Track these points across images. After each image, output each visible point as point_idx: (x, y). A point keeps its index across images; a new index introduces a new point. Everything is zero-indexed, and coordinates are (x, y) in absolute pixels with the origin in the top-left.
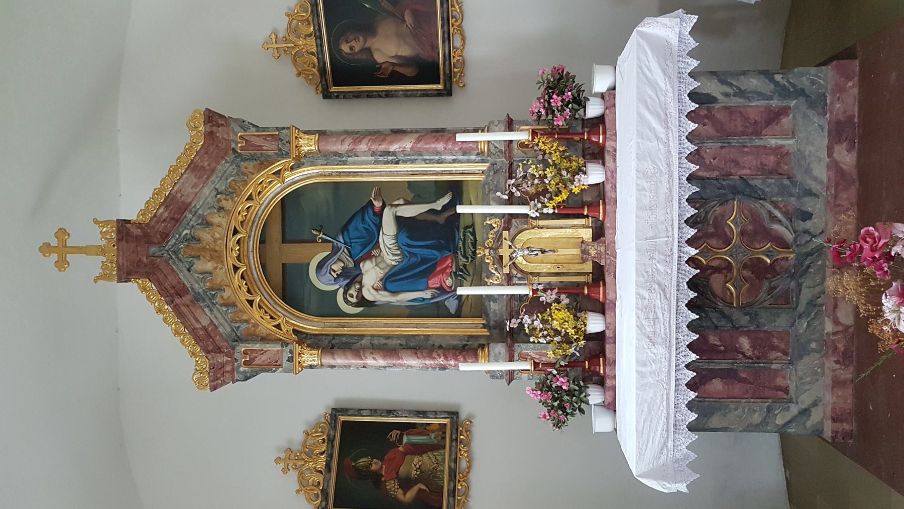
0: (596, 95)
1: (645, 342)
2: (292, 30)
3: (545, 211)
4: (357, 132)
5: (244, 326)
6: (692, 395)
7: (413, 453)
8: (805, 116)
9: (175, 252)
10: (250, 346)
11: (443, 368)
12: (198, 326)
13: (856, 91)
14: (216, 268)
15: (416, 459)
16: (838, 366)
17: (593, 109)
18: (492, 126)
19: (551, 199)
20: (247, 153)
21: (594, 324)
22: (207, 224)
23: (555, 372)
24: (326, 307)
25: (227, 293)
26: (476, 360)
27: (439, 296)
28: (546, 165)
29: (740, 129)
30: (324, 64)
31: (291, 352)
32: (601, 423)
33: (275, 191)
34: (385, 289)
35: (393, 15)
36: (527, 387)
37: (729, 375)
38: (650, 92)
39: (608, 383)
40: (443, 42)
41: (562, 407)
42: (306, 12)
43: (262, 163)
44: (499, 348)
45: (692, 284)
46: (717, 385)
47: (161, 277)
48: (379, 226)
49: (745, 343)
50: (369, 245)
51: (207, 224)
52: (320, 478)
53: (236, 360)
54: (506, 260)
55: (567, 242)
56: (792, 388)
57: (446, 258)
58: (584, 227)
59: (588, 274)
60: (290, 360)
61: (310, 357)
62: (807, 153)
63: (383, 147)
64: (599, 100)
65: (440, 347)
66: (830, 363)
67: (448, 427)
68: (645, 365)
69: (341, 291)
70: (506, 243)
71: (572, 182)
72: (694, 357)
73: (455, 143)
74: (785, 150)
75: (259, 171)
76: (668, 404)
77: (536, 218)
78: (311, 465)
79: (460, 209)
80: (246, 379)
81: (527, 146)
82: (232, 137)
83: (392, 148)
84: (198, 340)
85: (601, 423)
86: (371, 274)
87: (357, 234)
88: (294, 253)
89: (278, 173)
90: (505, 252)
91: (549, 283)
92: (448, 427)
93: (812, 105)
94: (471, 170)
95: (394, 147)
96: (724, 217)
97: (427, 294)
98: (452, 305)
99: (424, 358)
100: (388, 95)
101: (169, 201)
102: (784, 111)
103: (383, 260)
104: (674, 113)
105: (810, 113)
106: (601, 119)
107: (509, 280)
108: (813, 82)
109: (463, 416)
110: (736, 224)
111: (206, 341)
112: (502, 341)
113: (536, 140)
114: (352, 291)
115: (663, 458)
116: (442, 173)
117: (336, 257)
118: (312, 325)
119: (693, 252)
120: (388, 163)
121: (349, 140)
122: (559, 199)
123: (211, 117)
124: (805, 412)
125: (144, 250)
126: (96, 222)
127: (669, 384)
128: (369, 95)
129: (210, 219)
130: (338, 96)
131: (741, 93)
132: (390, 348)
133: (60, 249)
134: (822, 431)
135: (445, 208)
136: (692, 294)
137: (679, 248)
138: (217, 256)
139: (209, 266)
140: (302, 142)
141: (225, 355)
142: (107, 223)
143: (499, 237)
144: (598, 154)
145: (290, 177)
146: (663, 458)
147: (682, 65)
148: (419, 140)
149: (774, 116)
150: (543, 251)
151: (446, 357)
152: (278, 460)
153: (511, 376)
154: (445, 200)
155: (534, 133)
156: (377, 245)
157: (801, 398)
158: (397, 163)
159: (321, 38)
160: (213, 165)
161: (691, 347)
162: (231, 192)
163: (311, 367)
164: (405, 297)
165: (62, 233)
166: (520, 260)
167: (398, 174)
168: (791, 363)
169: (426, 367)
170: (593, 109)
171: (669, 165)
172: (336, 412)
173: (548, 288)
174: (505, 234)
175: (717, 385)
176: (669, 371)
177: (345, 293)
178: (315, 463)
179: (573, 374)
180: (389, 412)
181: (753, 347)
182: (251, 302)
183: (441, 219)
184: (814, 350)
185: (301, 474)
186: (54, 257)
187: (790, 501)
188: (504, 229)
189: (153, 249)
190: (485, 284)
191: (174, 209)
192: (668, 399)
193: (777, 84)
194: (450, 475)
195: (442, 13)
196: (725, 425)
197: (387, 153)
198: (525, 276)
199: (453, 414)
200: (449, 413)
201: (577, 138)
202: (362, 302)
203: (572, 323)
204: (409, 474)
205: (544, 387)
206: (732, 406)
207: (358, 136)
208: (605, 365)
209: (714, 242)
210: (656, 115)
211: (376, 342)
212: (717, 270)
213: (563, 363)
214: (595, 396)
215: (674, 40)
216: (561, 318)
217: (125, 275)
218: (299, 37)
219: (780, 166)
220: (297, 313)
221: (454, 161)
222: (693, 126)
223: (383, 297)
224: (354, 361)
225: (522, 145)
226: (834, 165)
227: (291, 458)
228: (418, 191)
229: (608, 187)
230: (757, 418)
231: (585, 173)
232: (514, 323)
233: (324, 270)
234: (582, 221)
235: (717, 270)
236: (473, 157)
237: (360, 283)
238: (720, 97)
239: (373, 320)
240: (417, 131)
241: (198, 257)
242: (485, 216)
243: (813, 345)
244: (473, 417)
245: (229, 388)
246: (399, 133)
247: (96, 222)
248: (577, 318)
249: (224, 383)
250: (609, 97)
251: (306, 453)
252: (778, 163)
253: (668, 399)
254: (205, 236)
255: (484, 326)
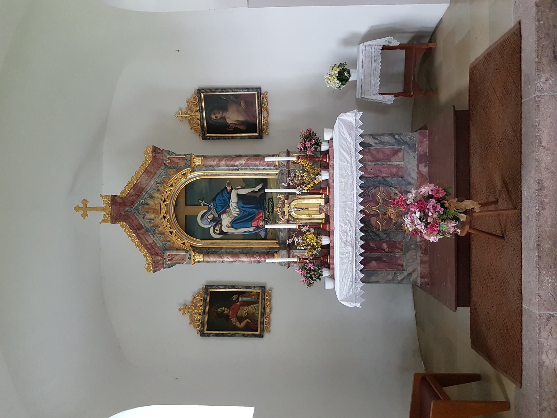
0: (326, 141)
1: (343, 245)
2: (189, 108)
3: (303, 191)
4: (220, 156)
5: (169, 243)
6: (362, 267)
7: (245, 306)
8: (408, 152)
9: (137, 210)
10: (171, 252)
11: (259, 262)
12: (147, 243)
13: (427, 142)
14: (156, 217)
15: (245, 308)
16: (422, 255)
17: (324, 147)
18: (281, 154)
19: (306, 186)
20: (171, 165)
21: (325, 241)
22: (152, 197)
23: (308, 262)
24: (205, 235)
25: (161, 229)
26: (274, 258)
27: (257, 230)
28: (304, 171)
29: (382, 157)
30: (204, 124)
31: (190, 255)
32: (328, 285)
33: (182, 182)
34: (232, 227)
35: (235, 102)
36: (296, 270)
37: (379, 259)
38: (344, 143)
39: (331, 266)
40: (259, 115)
41: (311, 277)
42: (196, 100)
43: (177, 170)
44: (284, 252)
45: (362, 221)
46: (374, 263)
47: (131, 221)
48: (230, 198)
49: (385, 246)
50: (225, 207)
51: (152, 197)
52: (200, 317)
53: (165, 259)
54: (286, 213)
55: (314, 205)
56: (404, 264)
57: (260, 213)
58: (321, 198)
59: (322, 219)
60: (190, 258)
61: (199, 258)
62: (409, 167)
63: (232, 163)
64: (327, 143)
65: (257, 253)
66: (419, 254)
67: (261, 293)
68: (343, 254)
69: (212, 228)
70: (286, 206)
71: (315, 179)
72: (363, 251)
73: (264, 161)
74: (400, 166)
75: (176, 174)
76: (352, 271)
77: (299, 195)
78: (196, 311)
79: (266, 191)
80: (170, 267)
81: (296, 163)
82: (164, 158)
83: (236, 163)
84: (148, 249)
85: (328, 285)
86: (226, 220)
87: (219, 202)
88: (190, 211)
89: (184, 174)
90: (286, 209)
91: (306, 223)
92: (261, 293)
93: (410, 148)
94: (271, 174)
95: (237, 163)
96: (376, 194)
97: (251, 229)
98: (263, 234)
99: (250, 257)
100: (233, 138)
101: (135, 187)
102: (400, 150)
103: (231, 214)
104: (354, 151)
105: (409, 151)
106: (327, 152)
107: (288, 222)
108: (411, 139)
109: (268, 288)
110: (380, 197)
111: (151, 250)
112: (285, 249)
113: (299, 161)
114: (217, 228)
115: (351, 293)
116: (258, 175)
117: (210, 212)
118: (199, 244)
119: (362, 207)
120: (234, 170)
121: (217, 160)
122: (309, 186)
123: (155, 150)
124: (410, 274)
125: (124, 209)
126: (101, 196)
127: (353, 262)
128: (224, 138)
129: (153, 195)
130: (209, 138)
131: (381, 143)
132: (234, 253)
133: (84, 209)
134: (417, 283)
135: (259, 190)
136: (362, 225)
137: (357, 206)
138: (156, 212)
139: (153, 216)
140: (196, 161)
141: (160, 256)
142: (106, 196)
143: (284, 203)
144: (326, 167)
145: (190, 176)
146: (351, 293)
147: (356, 132)
148: (248, 160)
149: (395, 152)
150: (302, 209)
151: (260, 257)
152: (180, 309)
153: (289, 264)
154: (260, 187)
155: (299, 157)
156: (229, 207)
157: (408, 269)
158: (238, 170)
159: (202, 112)
160: (155, 171)
161: (362, 247)
162: (163, 183)
163: (198, 262)
164: (242, 230)
165: (85, 201)
166: (293, 213)
167: (238, 175)
168: (404, 254)
169: (251, 262)
170: (324, 147)
171: (352, 172)
172: (207, 287)
173: (306, 225)
174: (286, 201)
175: (374, 263)
176: (353, 257)
177: (214, 229)
178: (198, 310)
179: (316, 264)
180: (233, 287)
181: (388, 248)
182: (171, 233)
183: (258, 195)
184: (413, 249)
185: (191, 316)
186: (81, 212)
187: (417, 324)
188: (286, 199)
189: (127, 209)
190: (278, 223)
191: (137, 191)
192: (352, 268)
193: (396, 139)
194: (261, 315)
195: (258, 102)
196: (378, 280)
197: (234, 166)
198: (295, 220)
199: (263, 288)
200: (261, 287)
201: (317, 160)
202: (222, 233)
203: (315, 240)
204: (242, 315)
205: (303, 268)
206: (380, 272)
207: (221, 158)
208: (330, 259)
209: (372, 204)
210: (347, 152)
211: (228, 250)
212: (374, 215)
213: (311, 258)
214: (326, 273)
215: (353, 122)
216: (310, 238)
217: (114, 220)
218: (192, 112)
219: (399, 174)
220: (192, 238)
221: (264, 169)
222: (361, 156)
223: (231, 231)
224: (218, 259)
225: (293, 162)
226: (419, 173)
227: (185, 309)
228: (247, 183)
229: (331, 181)
230: (390, 277)
231: (321, 175)
232: (290, 241)
233: (204, 219)
234: (320, 196)
235: (374, 215)
236: (272, 168)
237: (221, 224)
238: (373, 144)
239: (227, 241)
240: (247, 156)
241: (148, 212)
242: (277, 193)
243: (413, 246)
244: (272, 288)
245: (163, 272)
246: (239, 157)
247: (101, 196)
248: (317, 238)
249: (159, 269)
250: (331, 142)
251: (193, 306)
252: (397, 172)
253: (352, 268)
254: (151, 202)
255: (277, 243)
